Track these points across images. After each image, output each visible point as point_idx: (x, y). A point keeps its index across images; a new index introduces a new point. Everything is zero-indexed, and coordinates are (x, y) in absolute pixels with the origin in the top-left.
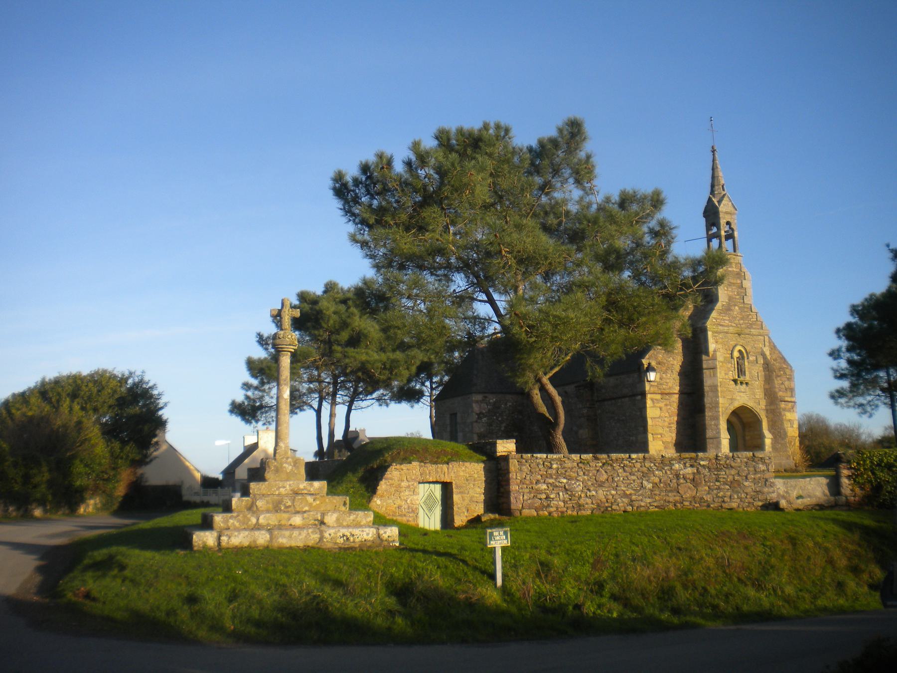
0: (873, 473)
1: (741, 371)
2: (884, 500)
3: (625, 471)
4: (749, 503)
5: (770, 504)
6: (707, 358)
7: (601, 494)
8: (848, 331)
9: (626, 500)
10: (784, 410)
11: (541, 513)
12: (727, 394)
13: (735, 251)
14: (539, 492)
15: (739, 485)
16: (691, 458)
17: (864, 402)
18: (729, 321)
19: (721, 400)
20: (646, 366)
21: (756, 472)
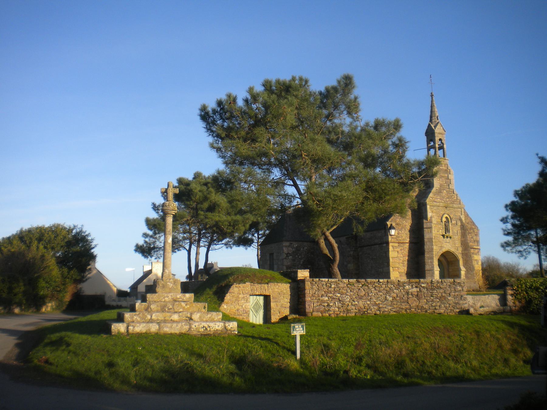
0: (527, 293)
1: (447, 230)
2: (533, 309)
3: (375, 289)
5: (463, 311)
7: (361, 303)
9: (376, 307)
10: (473, 253)
11: (324, 314)
12: (438, 244)
13: (444, 156)
14: (323, 301)
15: (445, 299)
16: (416, 282)
17: (522, 250)
18: (440, 199)
19: (435, 247)
20: (389, 226)
21: (455, 291)
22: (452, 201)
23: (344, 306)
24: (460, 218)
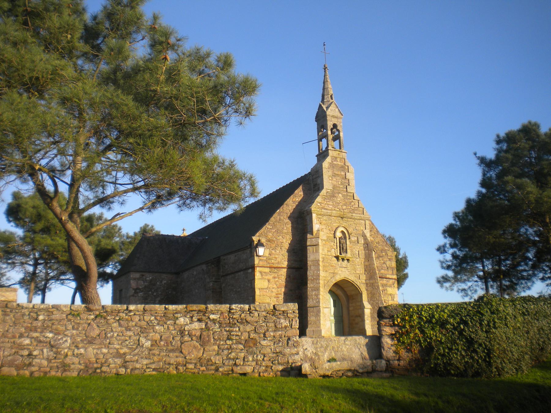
0: (422, 332)
1: (343, 249)
2: (436, 364)
3: (120, 325)
4: (267, 367)
5: (292, 368)
6: (311, 236)
7: (91, 352)
8: (450, 231)
9: (119, 361)
11: (21, 372)
12: (327, 269)
13: (340, 148)
14: (21, 347)
15: (255, 344)
16: (199, 311)
17: (466, 287)
18: (333, 205)
19: (322, 274)
20: (256, 243)
21: (276, 329)
22: (350, 210)
23: (59, 356)
24: (363, 232)
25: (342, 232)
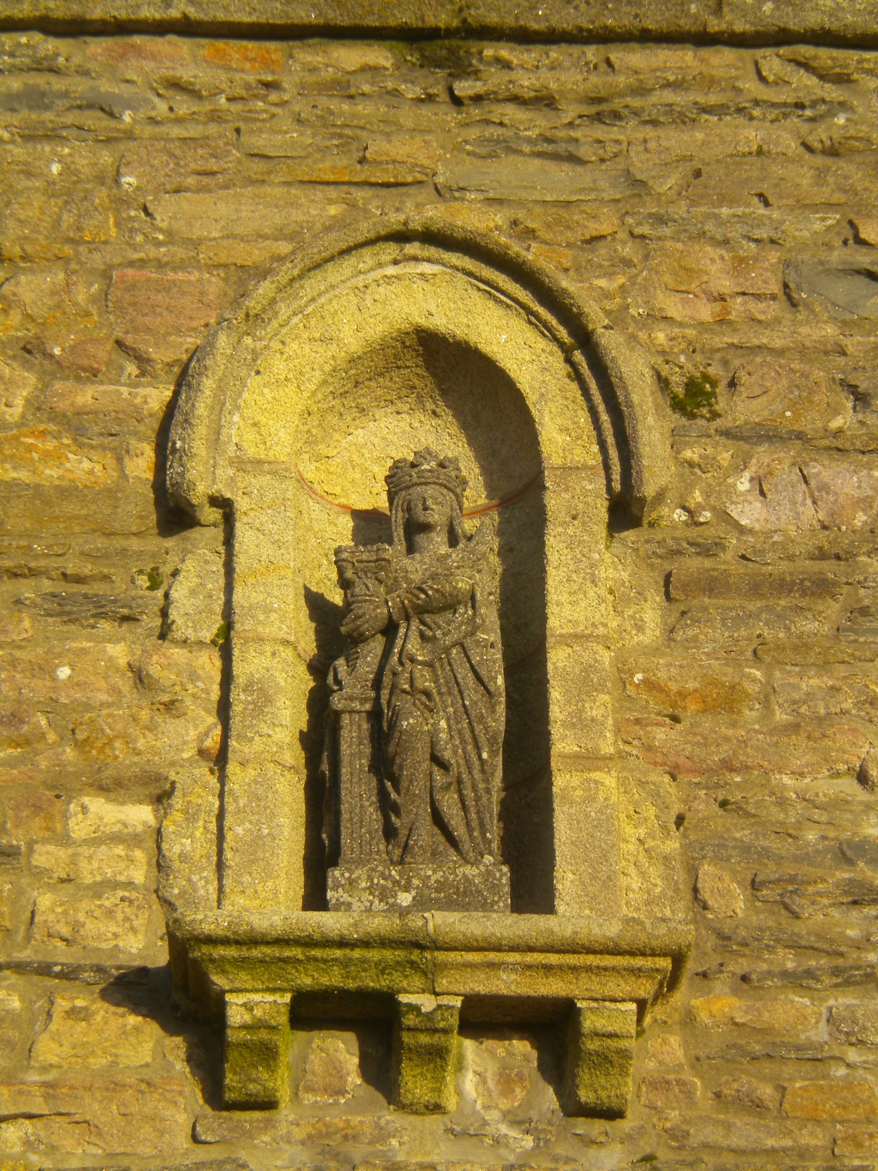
25: (450, 369)
